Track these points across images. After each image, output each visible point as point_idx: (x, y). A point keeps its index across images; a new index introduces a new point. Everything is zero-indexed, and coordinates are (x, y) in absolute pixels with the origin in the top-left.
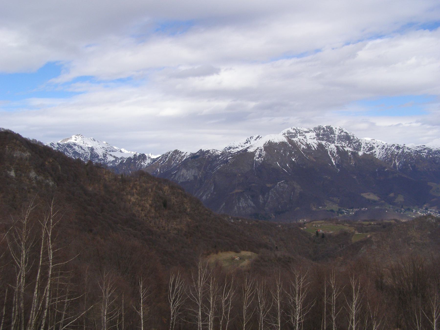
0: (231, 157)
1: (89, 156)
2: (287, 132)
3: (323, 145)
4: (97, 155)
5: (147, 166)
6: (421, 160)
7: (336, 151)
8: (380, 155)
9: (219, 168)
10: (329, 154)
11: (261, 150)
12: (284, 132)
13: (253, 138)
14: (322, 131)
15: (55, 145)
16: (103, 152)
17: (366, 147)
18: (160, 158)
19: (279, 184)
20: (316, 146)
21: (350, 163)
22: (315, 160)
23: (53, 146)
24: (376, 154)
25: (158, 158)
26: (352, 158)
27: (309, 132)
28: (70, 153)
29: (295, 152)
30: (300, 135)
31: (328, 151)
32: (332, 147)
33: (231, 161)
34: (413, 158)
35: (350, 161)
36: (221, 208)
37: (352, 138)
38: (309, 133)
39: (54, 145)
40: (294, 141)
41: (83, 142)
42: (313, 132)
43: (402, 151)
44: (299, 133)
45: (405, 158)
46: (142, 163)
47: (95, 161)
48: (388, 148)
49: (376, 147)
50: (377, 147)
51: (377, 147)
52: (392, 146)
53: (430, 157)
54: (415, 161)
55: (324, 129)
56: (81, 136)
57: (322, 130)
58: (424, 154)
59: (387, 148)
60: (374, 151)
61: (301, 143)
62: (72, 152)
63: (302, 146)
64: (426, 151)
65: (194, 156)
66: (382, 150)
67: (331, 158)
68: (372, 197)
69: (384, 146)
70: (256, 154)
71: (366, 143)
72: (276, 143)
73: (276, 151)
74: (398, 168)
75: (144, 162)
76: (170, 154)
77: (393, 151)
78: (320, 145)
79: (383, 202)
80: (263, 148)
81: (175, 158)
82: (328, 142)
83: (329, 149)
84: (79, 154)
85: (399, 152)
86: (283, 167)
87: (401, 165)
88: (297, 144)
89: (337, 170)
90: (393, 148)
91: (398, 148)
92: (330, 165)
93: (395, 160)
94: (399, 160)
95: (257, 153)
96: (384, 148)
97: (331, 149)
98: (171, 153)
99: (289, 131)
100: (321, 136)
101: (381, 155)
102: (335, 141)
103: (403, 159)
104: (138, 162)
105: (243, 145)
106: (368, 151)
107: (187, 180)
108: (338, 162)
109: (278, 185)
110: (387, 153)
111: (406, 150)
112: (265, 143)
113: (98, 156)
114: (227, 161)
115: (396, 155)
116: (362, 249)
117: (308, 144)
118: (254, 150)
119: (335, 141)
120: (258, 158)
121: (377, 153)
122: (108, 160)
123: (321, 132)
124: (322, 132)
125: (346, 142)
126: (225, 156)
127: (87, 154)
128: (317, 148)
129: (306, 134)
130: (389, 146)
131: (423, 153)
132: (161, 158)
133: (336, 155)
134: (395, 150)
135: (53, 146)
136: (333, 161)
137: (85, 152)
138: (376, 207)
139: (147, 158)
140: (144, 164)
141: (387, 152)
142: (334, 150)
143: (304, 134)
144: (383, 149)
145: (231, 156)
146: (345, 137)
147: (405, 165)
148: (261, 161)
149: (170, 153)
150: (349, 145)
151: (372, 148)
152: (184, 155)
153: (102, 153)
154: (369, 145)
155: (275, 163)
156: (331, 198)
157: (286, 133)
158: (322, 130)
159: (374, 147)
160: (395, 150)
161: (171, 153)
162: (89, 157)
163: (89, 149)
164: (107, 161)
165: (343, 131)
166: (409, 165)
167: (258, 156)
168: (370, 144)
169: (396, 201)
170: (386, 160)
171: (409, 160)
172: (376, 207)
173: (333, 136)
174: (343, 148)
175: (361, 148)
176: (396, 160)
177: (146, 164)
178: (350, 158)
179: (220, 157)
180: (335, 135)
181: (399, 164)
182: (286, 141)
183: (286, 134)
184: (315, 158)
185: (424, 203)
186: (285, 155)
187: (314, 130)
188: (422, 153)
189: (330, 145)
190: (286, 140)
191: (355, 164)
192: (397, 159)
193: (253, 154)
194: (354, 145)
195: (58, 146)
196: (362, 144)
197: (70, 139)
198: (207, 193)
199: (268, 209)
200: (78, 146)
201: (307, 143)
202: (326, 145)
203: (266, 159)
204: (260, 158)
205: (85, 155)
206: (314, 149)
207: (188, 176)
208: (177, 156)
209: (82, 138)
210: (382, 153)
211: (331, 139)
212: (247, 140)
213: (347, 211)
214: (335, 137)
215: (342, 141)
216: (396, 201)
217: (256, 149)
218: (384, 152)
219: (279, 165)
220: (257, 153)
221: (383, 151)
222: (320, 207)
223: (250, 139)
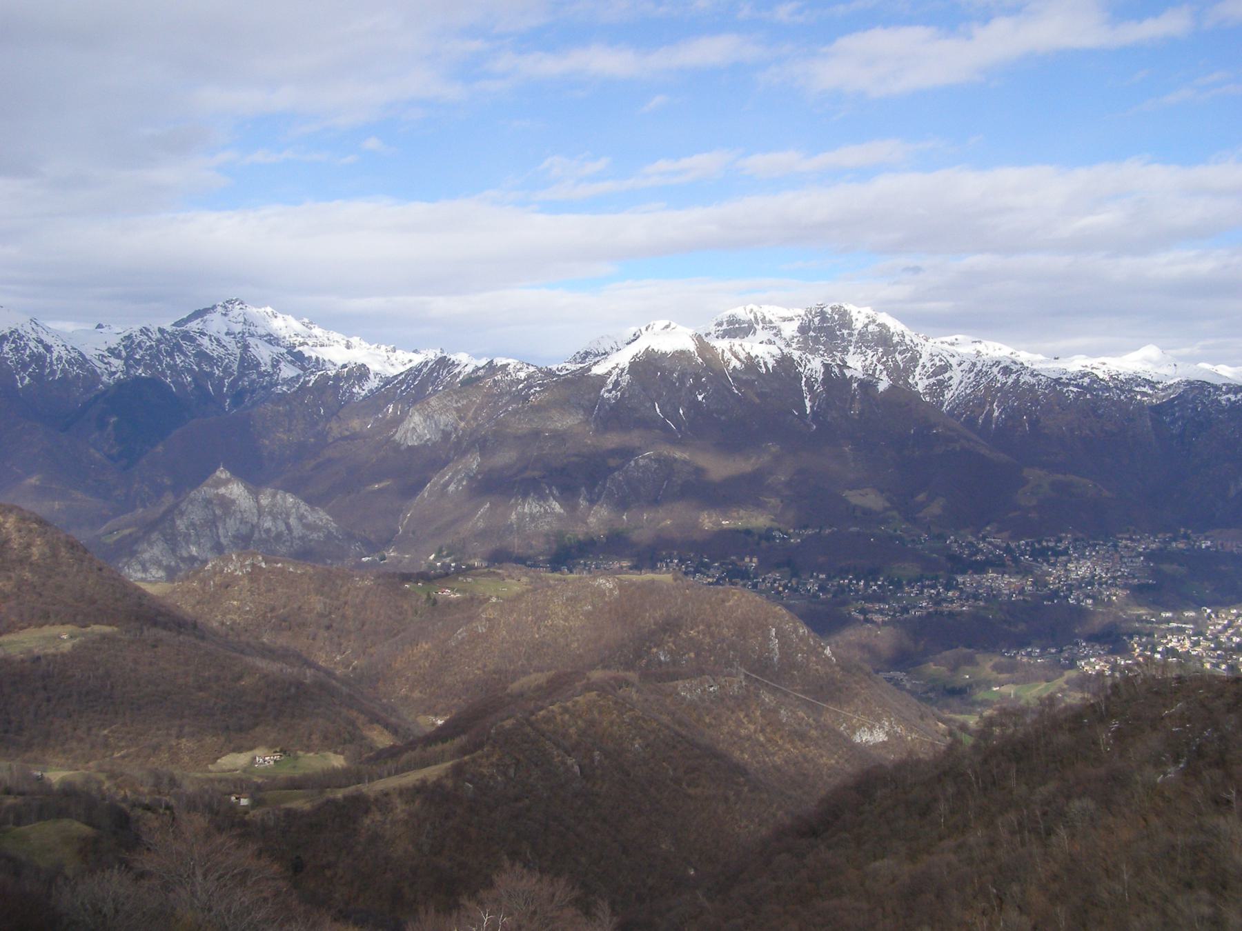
0: (540, 388)
1: (237, 363)
2: (726, 319)
3: (794, 361)
4: (255, 362)
5: (366, 397)
6: (1059, 405)
7: (821, 377)
8: (959, 388)
9: (502, 415)
10: (803, 384)
12: (719, 320)
13: (652, 328)
15: (152, 334)
16: (271, 354)
17: (929, 365)
18: (400, 378)
21: (851, 409)
22: (757, 401)
23: (147, 335)
24: (952, 383)
25: (396, 377)
26: (858, 397)
28: (190, 354)
29: (709, 378)
30: (763, 327)
31: (803, 376)
33: (536, 398)
34: (1037, 400)
35: (851, 404)
36: (478, 516)
37: (896, 339)
38: (792, 322)
39: (150, 334)
40: (716, 349)
41: (243, 320)
43: (1015, 380)
45: (1017, 399)
46: (354, 390)
47: (248, 378)
48: (984, 369)
49: (955, 366)
50: (960, 365)
51: (960, 365)
52: (994, 365)
54: (1041, 407)
56: (239, 304)
57: (819, 318)
58: (1071, 390)
60: (947, 375)
62: (193, 352)
64: (1087, 380)
65: (471, 377)
66: (969, 373)
67: (805, 395)
69: (974, 365)
70: (609, 380)
71: (931, 354)
73: (659, 374)
74: (996, 424)
75: (360, 387)
76: (429, 367)
77: (994, 380)
79: (895, 513)
81: (437, 377)
82: (807, 354)
83: (806, 371)
84: (212, 358)
85: (1007, 382)
86: (666, 416)
87: (1003, 416)
88: (723, 356)
89: (809, 427)
90: (995, 370)
91: (1006, 371)
92: (797, 414)
95: (613, 378)
96: (973, 371)
97: (810, 371)
98: (430, 364)
101: (963, 389)
102: (851, 345)
104: (345, 386)
106: (932, 377)
107: (423, 442)
108: (819, 407)
112: (638, 352)
113: (259, 364)
116: (459, 631)
118: (606, 371)
119: (849, 348)
120: (610, 393)
122: (280, 375)
123: (813, 321)
124: (817, 323)
125: (877, 351)
127: (232, 358)
128: (773, 367)
130: (987, 366)
132: (403, 376)
133: (817, 389)
134: (999, 377)
135: (147, 335)
136: (808, 404)
137: (228, 354)
139: (371, 376)
140: (360, 391)
141: (978, 382)
142: (817, 375)
144: (971, 371)
145: (541, 386)
146: (876, 336)
147: (1012, 415)
148: (614, 399)
149: (427, 365)
150: (885, 359)
152: (460, 372)
153: (270, 358)
154: (937, 359)
157: (724, 320)
158: (819, 318)
160: (999, 377)
161: (430, 364)
162: (236, 366)
163: (239, 345)
164: (278, 379)
165: (874, 321)
166: (1025, 417)
167: (611, 387)
168: (940, 356)
170: (969, 401)
171: (1026, 405)
173: (845, 332)
175: (915, 367)
176: (995, 404)
177: (363, 390)
178: (854, 396)
180: (853, 330)
181: (1001, 413)
182: (692, 350)
183: (725, 323)
185: (988, 524)
186: (682, 383)
189: (809, 361)
191: (861, 414)
192: (999, 402)
193: (602, 379)
195: (159, 336)
196: (922, 356)
197: (212, 311)
198: (459, 477)
199: (595, 520)
200: (210, 336)
201: (751, 354)
202: (802, 361)
203: (627, 396)
205: (227, 360)
207: (426, 432)
208: (442, 374)
209: (241, 309)
210: (966, 383)
211: (839, 342)
212: (635, 335)
214: (850, 335)
217: (612, 368)
218: (971, 379)
219: (658, 410)
220: (611, 377)
221: (969, 378)
222: (723, 522)
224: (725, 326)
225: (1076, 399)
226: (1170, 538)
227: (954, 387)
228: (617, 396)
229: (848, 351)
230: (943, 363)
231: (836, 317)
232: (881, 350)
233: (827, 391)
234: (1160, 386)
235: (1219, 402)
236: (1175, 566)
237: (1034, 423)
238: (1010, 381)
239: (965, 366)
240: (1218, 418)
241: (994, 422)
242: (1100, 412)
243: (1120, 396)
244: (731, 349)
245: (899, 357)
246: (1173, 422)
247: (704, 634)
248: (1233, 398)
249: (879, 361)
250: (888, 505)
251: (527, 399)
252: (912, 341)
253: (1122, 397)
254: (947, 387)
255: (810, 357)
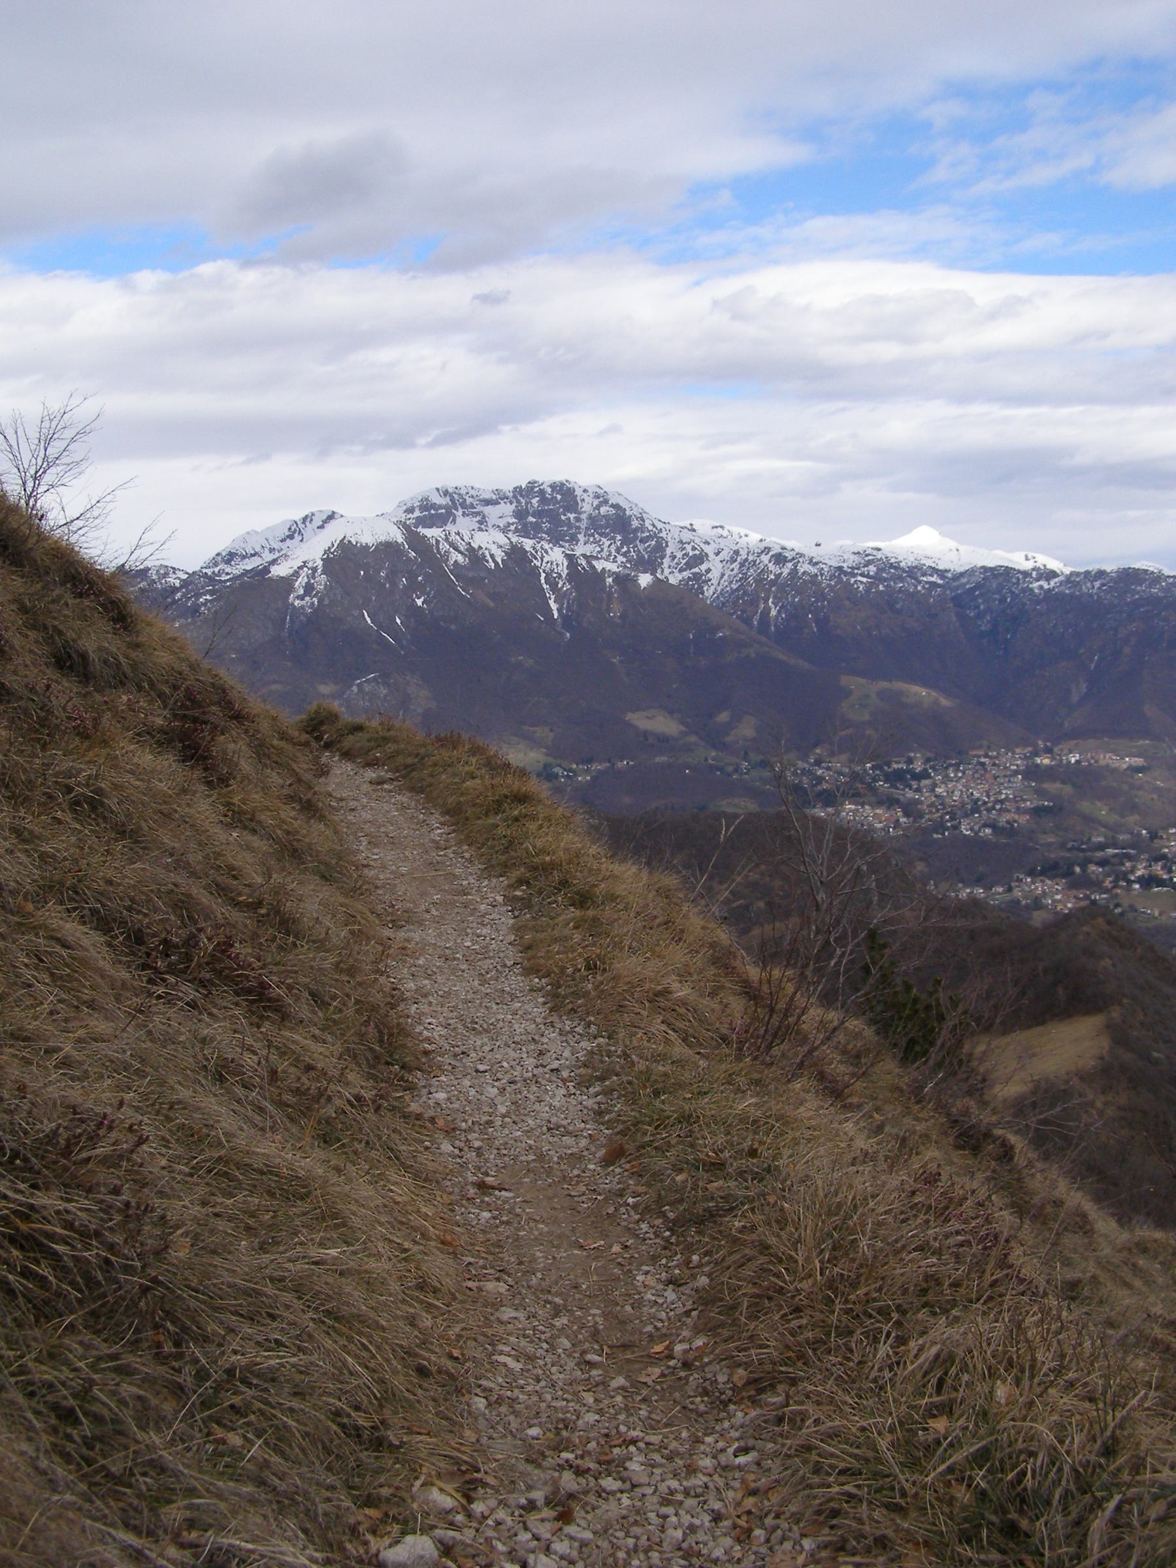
6: (849, 599)
7: (566, 571)
10: (543, 581)
11: (314, 570)
14: (535, 501)
17: (679, 555)
19: (358, 685)
20: (500, 556)
27: (496, 503)
29: (427, 577)
32: (555, 557)
33: (209, 610)
37: (635, 524)
42: (511, 503)
44: (463, 505)
45: (798, 593)
48: (751, 558)
49: (712, 556)
51: (717, 554)
53: (878, 592)
55: (542, 493)
59: (746, 560)
60: (704, 567)
61: (452, 545)
63: (456, 557)
64: (872, 569)
68: (662, 724)
69: (737, 552)
70: (297, 584)
71: (681, 542)
72: (366, 547)
74: (775, 626)
78: (516, 554)
79: (693, 739)
80: (320, 563)
86: (380, 627)
88: (438, 548)
89: (562, 635)
90: (765, 558)
91: (779, 559)
93: (766, 600)
94: (780, 599)
95: (302, 581)
99: (427, 499)
100: (531, 519)
103: (794, 597)
105: (276, 546)
106: (685, 570)
108: (568, 608)
109: (355, 689)
110: (745, 577)
111: (804, 567)
114: (195, 610)
115: (773, 583)
117: (476, 547)
118: (291, 571)
120: (303, 599)
121: (714, 575)
125: (614, 538)
126: (192, 590)
128: (503, 560)
129: (488, 510)
131: (859, 578)
134: (771, 567)
136: (554, 606)
138: (657, 760)
143: (479, 508)
144: (733, 561)
145: (211, 593)
147: (795, 615)
150: (625, 549)
151: (701, 558)
154: (689, 548)
155: (356, 613)
156: (525, 728)
159: (707, 555)
160: (771, 567)
165: (606, 502)
167: (301, 592)
169: (729, 739)
170: (739, 599)
172: (657, 760)
173: (572, 516)
174: (589, 563)
175: (663, 557)
178: (610, 594)
179: (179, 595)
180: (580, 513)
182: (400, 540)
184: (494, 596)
185: (816, 745)
186: (394, 584)
187: (515, 497)
188: (855, 575)
189: (547, 552)
190: (398, 537)
191: (622, 617)
192: (775, 597)
193: (287, 583)
194: (641, 547)
203: (326, 602)
204: (307, 598)
206: (493, 565)
213: (570, 770)
214: (578, 519)
215: (601, 535)
216: (729, 739)
219: (368, 620)
223: (301, 526)
224: (417, 514)
225: (868, 590)
226: (1031, 753)
227: (714, 582)
228: (313, 603)
229: (578, 541)
230: (697, 552)
231: (559, 497)
232: (619, 537)
233: (577, 587)
234: (949, 575)
235: (1032, 590)
236: (1058, 785)
237: (823, 623)
238: (786, 571)
239: (725, 555)
240: (1035, 609)
241: (772, 623)
242: (898, 606)
243: (916, 587)
244: (447, 540)
245: (641, 547)
246: (980, 616)
247: (771, 876)
248: (1046, 586)
249: (618, 550)
250: (682, 728)
251: (197, 611)
252: (654, 525)
253: (919, 588)
254: (706, 582)
255: (546, 546)
